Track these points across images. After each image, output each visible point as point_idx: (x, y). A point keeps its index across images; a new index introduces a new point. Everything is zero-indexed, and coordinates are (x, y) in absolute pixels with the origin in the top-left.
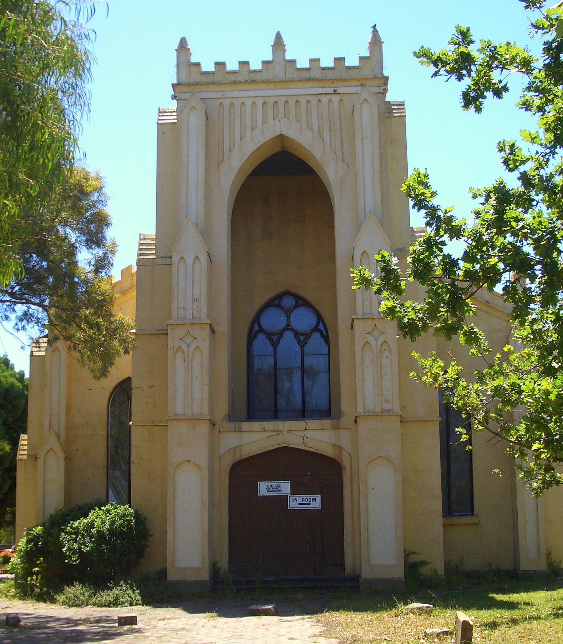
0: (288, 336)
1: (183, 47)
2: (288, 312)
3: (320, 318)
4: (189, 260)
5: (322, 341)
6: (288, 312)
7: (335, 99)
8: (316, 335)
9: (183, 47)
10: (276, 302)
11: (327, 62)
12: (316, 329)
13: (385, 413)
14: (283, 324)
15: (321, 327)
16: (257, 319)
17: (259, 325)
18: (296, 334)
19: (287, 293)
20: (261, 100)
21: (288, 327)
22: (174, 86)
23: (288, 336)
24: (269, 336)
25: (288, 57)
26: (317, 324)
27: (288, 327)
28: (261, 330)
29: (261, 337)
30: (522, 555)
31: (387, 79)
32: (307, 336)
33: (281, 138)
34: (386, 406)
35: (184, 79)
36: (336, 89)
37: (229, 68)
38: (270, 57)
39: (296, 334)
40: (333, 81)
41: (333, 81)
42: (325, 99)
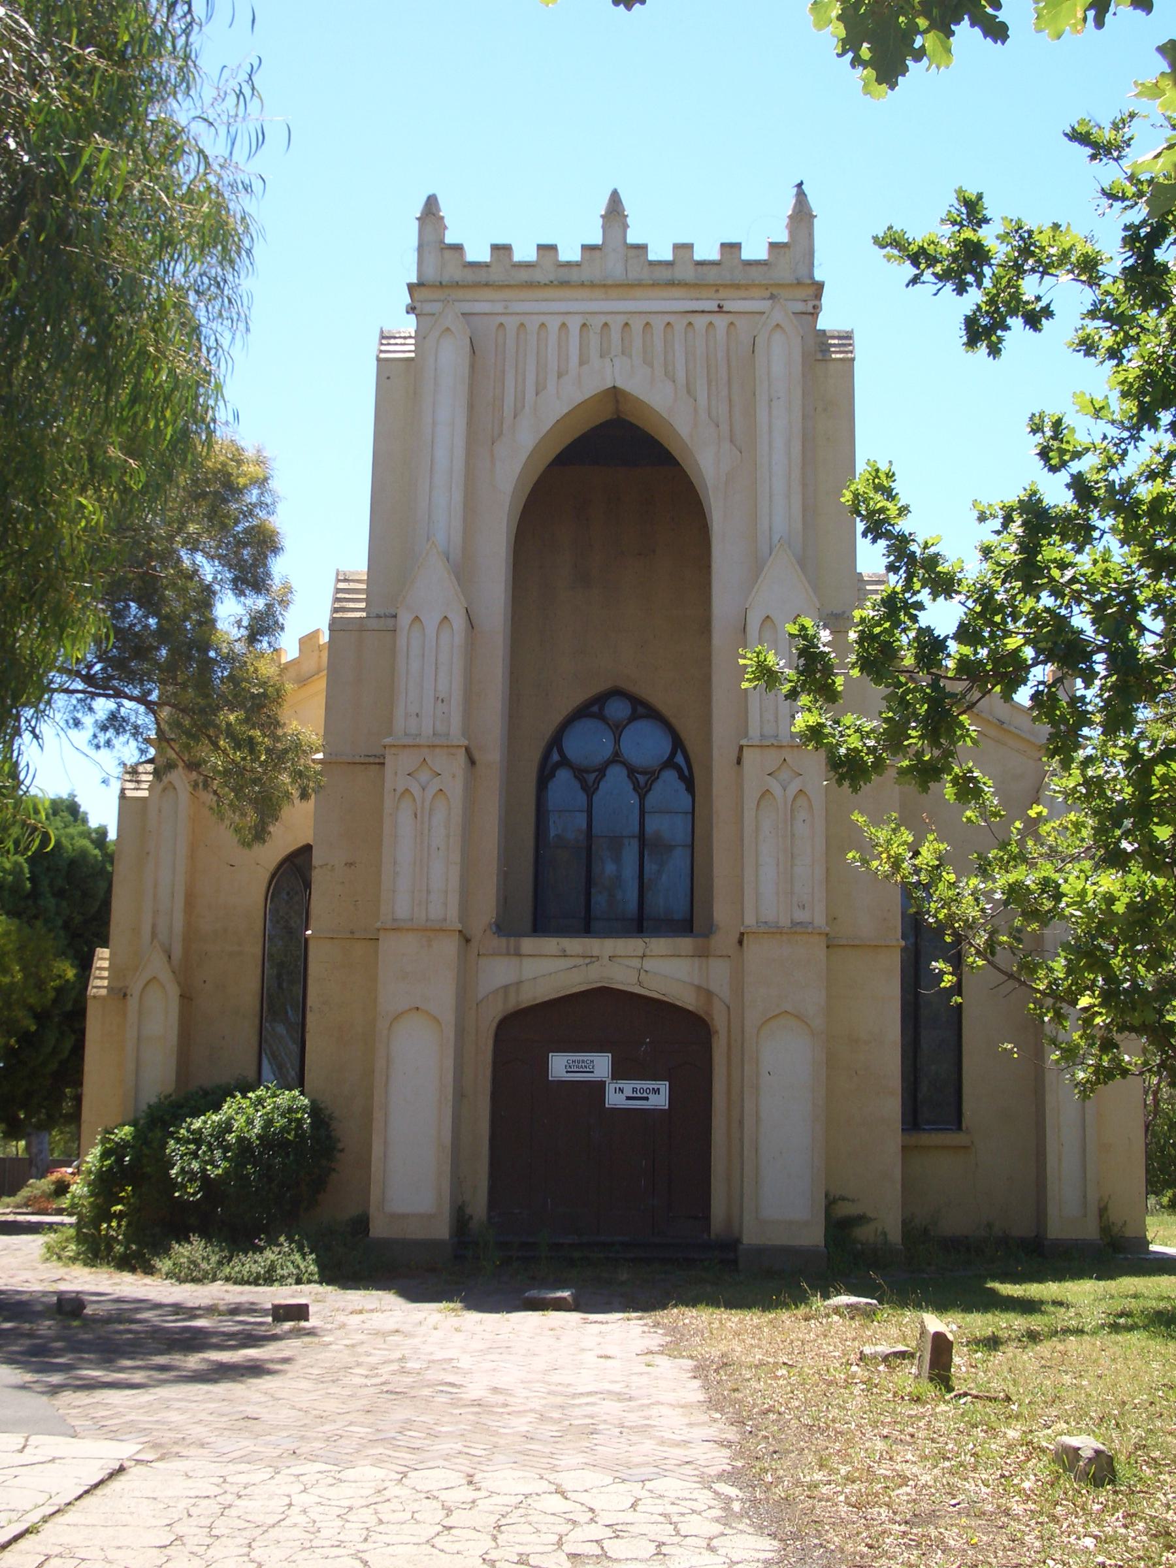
0: (616, 774)
1: (431, 213)
2: (617, 730)
3: (678, 743)
4: (431, 622)
5: (681, 786)
6: (617, 730)
7: (721, 322)
8: (670, 776)
9: (431, 213)
10: (595, 709)
11: (708, 251)
12: (669, 763)
13: (797, 928)
14: (607, 752)
15: (679, 759)
16: (556, 741)
17: (561, 752)
18: (632, 771)
19: (617, 693)
20: (621, 320)
21: (616, 758)
22: (411, 287)
23: (616, 774)
24: (580, 773)
25: (633, 238)
26: (673, 754)
27: (616, 758)
28: (565, 762)
29: (563, 775)
30: (1052, 1210)
31: (820, 286)
32: (653, 775)
33: (615, 393)
34: (801, 916)
35: (431, 275)
36: (722, 303)
37: (518, 256)
38: (596, 238)
39: (632, 771)
40: (717, 287)
41: (717, 287)
42: (700, 322)
